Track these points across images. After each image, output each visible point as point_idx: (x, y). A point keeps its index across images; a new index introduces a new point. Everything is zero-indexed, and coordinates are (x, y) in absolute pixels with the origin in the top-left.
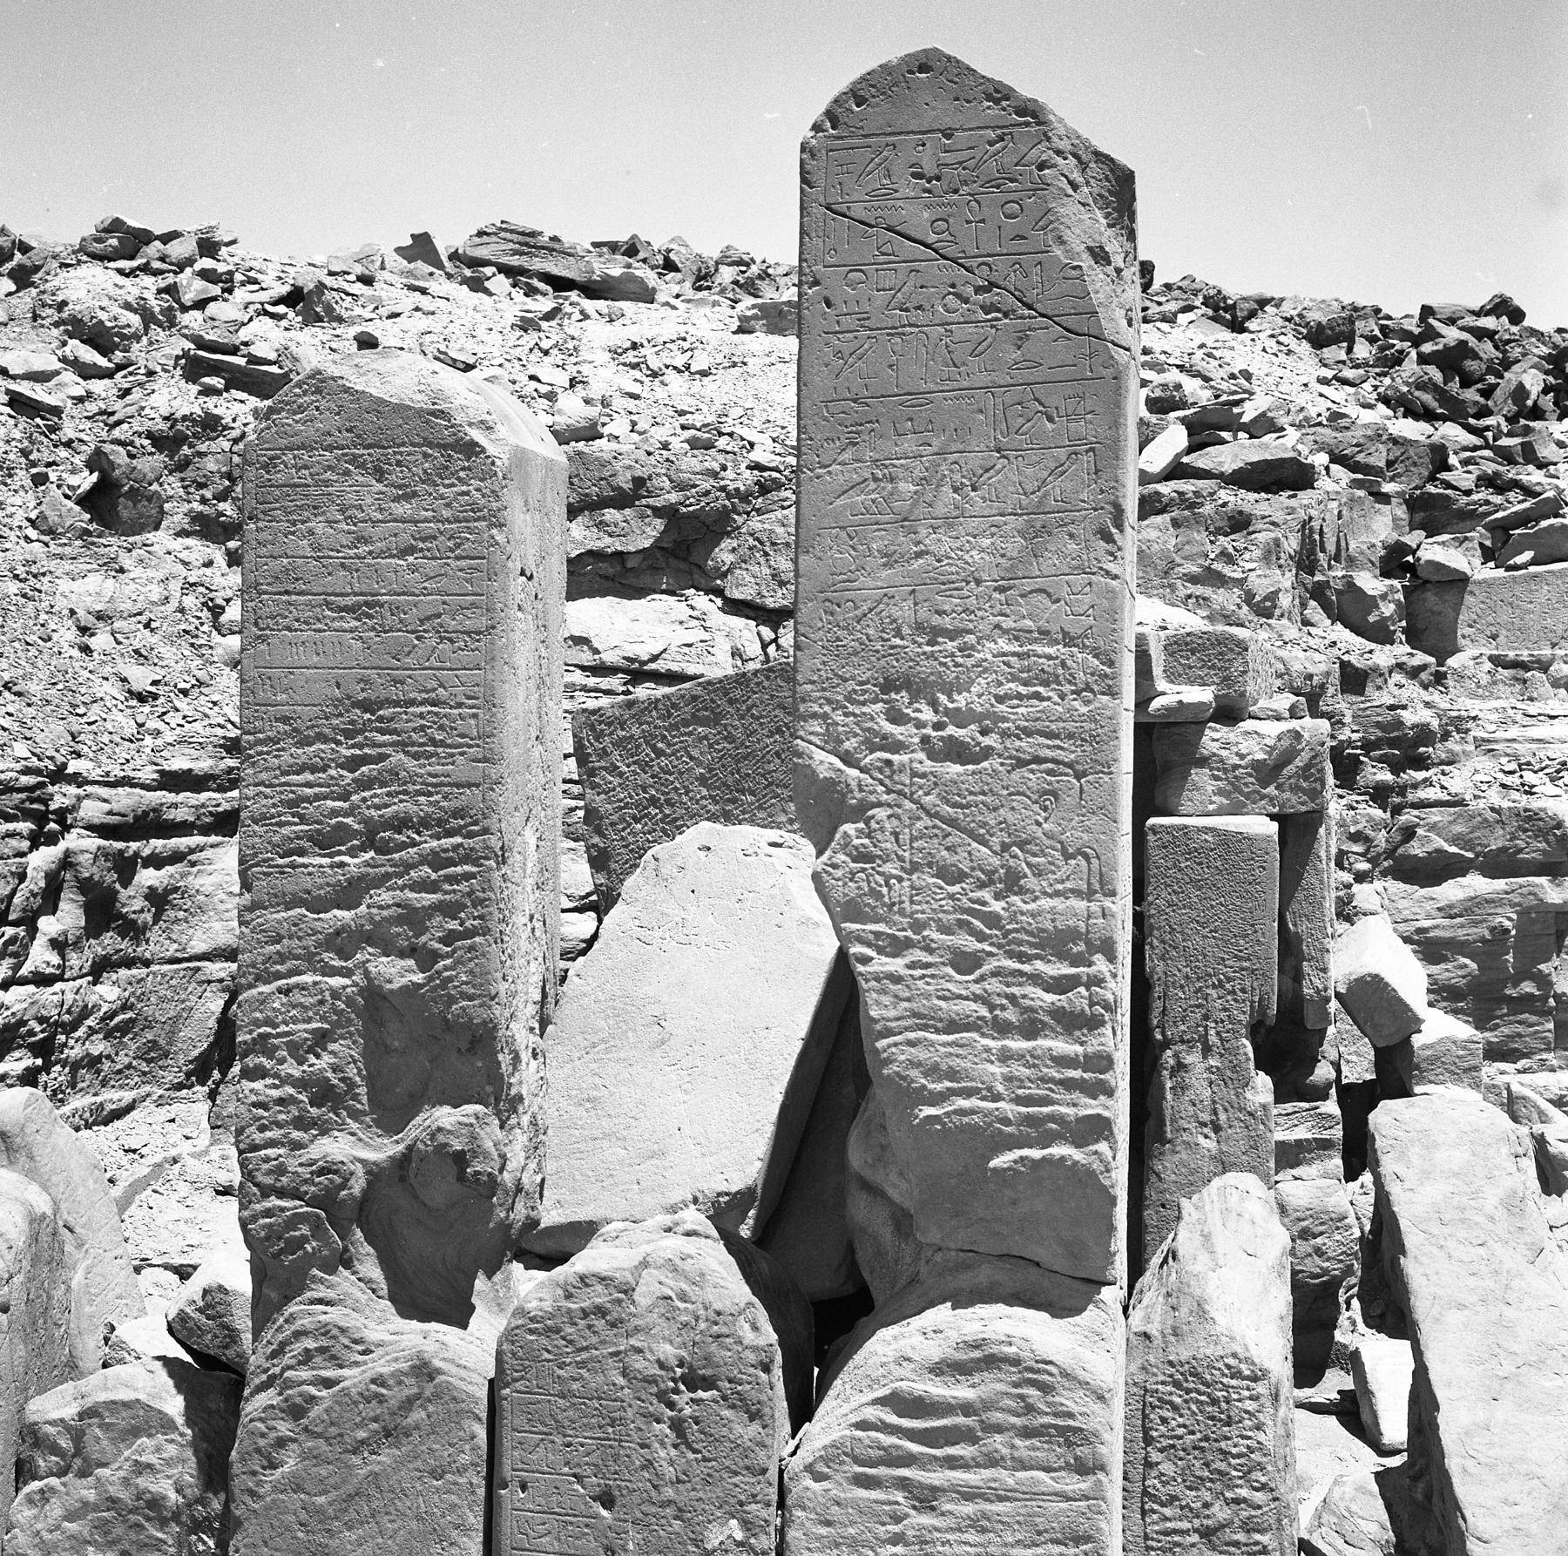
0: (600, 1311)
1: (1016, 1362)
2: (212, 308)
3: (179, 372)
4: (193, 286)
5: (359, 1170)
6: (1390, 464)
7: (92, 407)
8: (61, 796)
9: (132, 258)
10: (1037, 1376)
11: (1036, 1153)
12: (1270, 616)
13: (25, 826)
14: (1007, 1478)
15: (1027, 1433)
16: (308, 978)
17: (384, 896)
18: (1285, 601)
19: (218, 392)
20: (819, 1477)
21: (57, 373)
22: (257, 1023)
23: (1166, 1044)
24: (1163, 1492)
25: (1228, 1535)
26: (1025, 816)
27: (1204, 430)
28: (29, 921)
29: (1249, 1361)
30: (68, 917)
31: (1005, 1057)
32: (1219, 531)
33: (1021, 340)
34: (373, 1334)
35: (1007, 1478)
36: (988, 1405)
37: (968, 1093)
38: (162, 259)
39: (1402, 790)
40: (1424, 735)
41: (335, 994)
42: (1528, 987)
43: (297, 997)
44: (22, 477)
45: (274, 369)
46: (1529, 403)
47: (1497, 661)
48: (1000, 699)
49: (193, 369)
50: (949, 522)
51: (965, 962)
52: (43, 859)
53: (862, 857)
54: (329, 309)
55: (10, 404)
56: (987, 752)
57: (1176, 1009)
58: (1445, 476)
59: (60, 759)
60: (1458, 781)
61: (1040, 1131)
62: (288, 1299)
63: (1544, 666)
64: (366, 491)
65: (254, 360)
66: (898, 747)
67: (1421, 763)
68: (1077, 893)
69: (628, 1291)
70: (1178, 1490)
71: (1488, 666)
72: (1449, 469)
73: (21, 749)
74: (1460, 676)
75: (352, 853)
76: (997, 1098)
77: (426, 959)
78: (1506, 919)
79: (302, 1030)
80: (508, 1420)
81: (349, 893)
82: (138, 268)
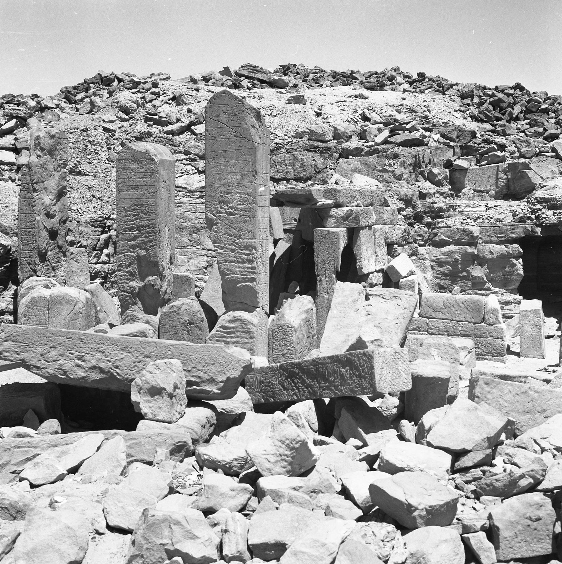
0: (175, 312)
1: (241, 320)
2: (154, 102)
3: (143, 120)
4: (149, 96)
5: (137, 288)
6: (458, 137)
7: (123, 129)
8: (108, 223)
9: (136, 89)
10: (245, 322)
11: (244, 284)
12: (400, 180)
13: (100, 229)
14: (240, 340)
15: (243, 332)
16: (128, 254)
17: (140, 239)
18: (405, 176)
19: (151, 126)
20: (211, 340)
21: (116, 121)
22: (120, 261)
23: (318, 275)
24: (276, 348)
25: (287, 355)
26: (241, 225)
27: (393, 133)
28: (101, 250)
29: (290, 324)
30: (110, 250)
31: (239, 267)
32: (391, 158)
33: (240, 141)
34: (140, 316)
35: (240, 340)
36: (237, 327)
37: (233, 273)
38: (143, 89)
39: (435, 224)
40: (441, 210)
41: (132, 256)
42: (465, 274)
43: (126, 257)
44: (105, 148)
45: (165, 119)
46: (514, 116)
47: (475, 190)
48: (238, 205)
49: (147, 120)
50: (229, 173)
51: (233, 251)
52: (104, 237)
53: (216, 232)
54: (183, 101)
55: (103, 130)
56: (236, 214)
57: (320, 268)
58: (474, 140)
59: (109, 214)
60: (450, 222)
61: (244, 280)
62: (126, 310)
63: (488, 192)
64: (136, 167)
65: (160, 117)
66: (222, 213)
67: (441, 217)
68: (250, 239)
69: (180, 308)
70: (278, 347)
71: (473, 191)
72: (476, 138)
73: (99, 212)
74: (464, 194)
75: (135, 231)
76: (238, 274)
77: (147, 250)
78: (458, 256)
79: (127, 263)
80: (161, 331)
81: (134, 239)
82: (137, 91)
